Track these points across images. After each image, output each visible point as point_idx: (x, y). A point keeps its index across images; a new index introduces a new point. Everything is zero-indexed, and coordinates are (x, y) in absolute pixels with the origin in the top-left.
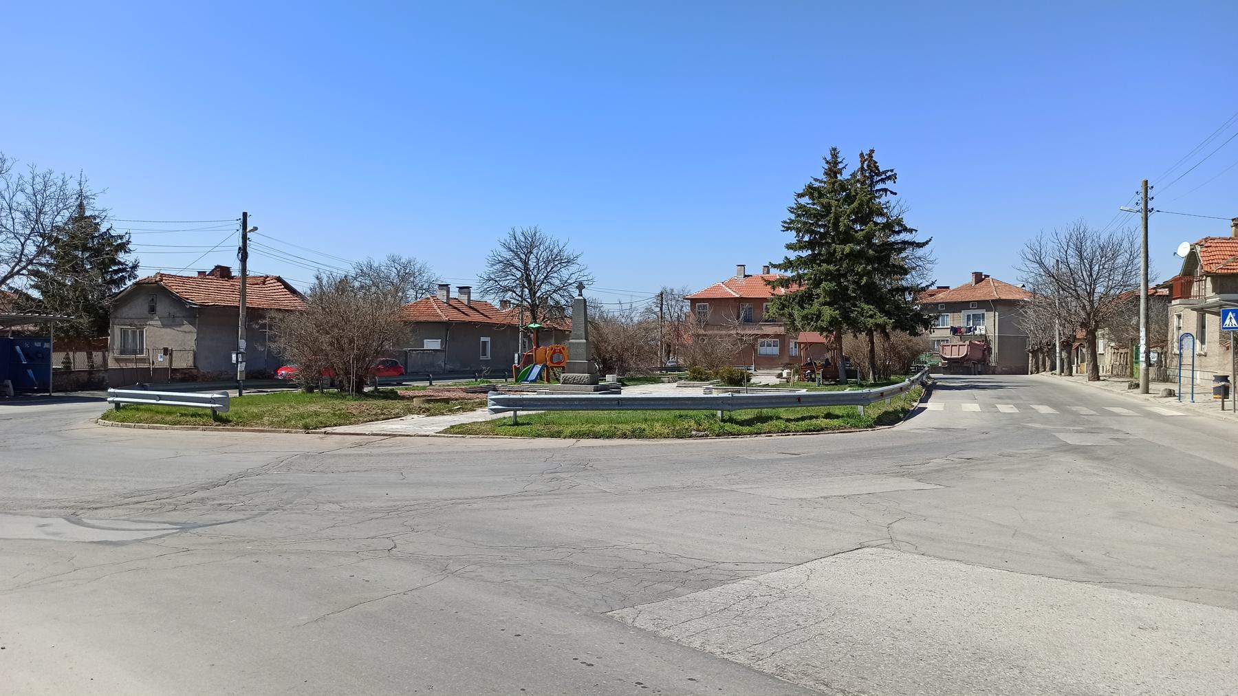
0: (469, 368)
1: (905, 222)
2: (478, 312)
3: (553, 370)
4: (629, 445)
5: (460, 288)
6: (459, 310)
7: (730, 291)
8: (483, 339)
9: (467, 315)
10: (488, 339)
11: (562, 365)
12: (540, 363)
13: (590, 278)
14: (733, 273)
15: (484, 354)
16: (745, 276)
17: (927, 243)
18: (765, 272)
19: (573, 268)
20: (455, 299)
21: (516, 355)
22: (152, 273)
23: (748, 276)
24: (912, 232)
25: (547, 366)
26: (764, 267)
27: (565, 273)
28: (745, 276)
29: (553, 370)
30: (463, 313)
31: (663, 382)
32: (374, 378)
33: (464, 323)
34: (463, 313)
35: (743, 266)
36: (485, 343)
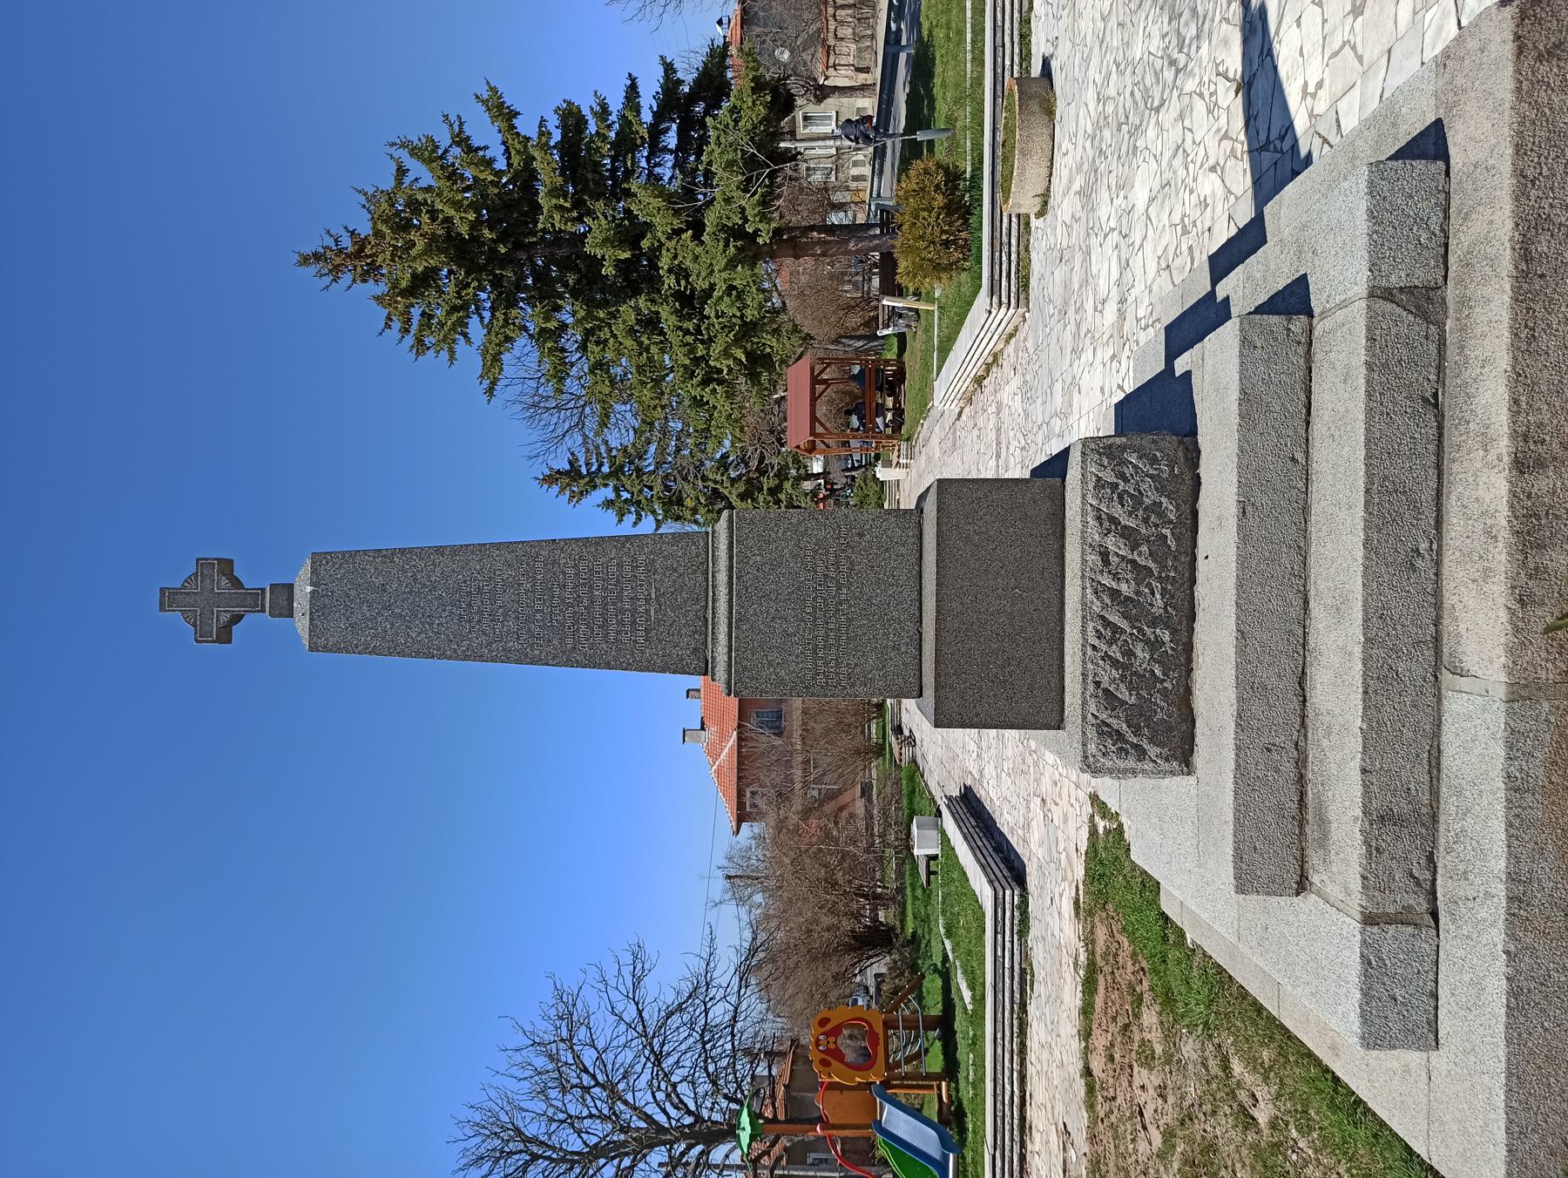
1: (484, 108)
3: (898, 1065)
4: (937, 661)
7: (726, 750)
11: (879, 1029)
12: (872, 1109)
13: (628, 959)
14: (697, 748)
16: (703, 728)
19: (591, 1001)
22: (698, 61)
23: (703, 724)
25: (886, 1084)
26: (688, 697)
27: (605, 1028)
28: (703, 728)
29: (898, 1065)
35: (684, 731)
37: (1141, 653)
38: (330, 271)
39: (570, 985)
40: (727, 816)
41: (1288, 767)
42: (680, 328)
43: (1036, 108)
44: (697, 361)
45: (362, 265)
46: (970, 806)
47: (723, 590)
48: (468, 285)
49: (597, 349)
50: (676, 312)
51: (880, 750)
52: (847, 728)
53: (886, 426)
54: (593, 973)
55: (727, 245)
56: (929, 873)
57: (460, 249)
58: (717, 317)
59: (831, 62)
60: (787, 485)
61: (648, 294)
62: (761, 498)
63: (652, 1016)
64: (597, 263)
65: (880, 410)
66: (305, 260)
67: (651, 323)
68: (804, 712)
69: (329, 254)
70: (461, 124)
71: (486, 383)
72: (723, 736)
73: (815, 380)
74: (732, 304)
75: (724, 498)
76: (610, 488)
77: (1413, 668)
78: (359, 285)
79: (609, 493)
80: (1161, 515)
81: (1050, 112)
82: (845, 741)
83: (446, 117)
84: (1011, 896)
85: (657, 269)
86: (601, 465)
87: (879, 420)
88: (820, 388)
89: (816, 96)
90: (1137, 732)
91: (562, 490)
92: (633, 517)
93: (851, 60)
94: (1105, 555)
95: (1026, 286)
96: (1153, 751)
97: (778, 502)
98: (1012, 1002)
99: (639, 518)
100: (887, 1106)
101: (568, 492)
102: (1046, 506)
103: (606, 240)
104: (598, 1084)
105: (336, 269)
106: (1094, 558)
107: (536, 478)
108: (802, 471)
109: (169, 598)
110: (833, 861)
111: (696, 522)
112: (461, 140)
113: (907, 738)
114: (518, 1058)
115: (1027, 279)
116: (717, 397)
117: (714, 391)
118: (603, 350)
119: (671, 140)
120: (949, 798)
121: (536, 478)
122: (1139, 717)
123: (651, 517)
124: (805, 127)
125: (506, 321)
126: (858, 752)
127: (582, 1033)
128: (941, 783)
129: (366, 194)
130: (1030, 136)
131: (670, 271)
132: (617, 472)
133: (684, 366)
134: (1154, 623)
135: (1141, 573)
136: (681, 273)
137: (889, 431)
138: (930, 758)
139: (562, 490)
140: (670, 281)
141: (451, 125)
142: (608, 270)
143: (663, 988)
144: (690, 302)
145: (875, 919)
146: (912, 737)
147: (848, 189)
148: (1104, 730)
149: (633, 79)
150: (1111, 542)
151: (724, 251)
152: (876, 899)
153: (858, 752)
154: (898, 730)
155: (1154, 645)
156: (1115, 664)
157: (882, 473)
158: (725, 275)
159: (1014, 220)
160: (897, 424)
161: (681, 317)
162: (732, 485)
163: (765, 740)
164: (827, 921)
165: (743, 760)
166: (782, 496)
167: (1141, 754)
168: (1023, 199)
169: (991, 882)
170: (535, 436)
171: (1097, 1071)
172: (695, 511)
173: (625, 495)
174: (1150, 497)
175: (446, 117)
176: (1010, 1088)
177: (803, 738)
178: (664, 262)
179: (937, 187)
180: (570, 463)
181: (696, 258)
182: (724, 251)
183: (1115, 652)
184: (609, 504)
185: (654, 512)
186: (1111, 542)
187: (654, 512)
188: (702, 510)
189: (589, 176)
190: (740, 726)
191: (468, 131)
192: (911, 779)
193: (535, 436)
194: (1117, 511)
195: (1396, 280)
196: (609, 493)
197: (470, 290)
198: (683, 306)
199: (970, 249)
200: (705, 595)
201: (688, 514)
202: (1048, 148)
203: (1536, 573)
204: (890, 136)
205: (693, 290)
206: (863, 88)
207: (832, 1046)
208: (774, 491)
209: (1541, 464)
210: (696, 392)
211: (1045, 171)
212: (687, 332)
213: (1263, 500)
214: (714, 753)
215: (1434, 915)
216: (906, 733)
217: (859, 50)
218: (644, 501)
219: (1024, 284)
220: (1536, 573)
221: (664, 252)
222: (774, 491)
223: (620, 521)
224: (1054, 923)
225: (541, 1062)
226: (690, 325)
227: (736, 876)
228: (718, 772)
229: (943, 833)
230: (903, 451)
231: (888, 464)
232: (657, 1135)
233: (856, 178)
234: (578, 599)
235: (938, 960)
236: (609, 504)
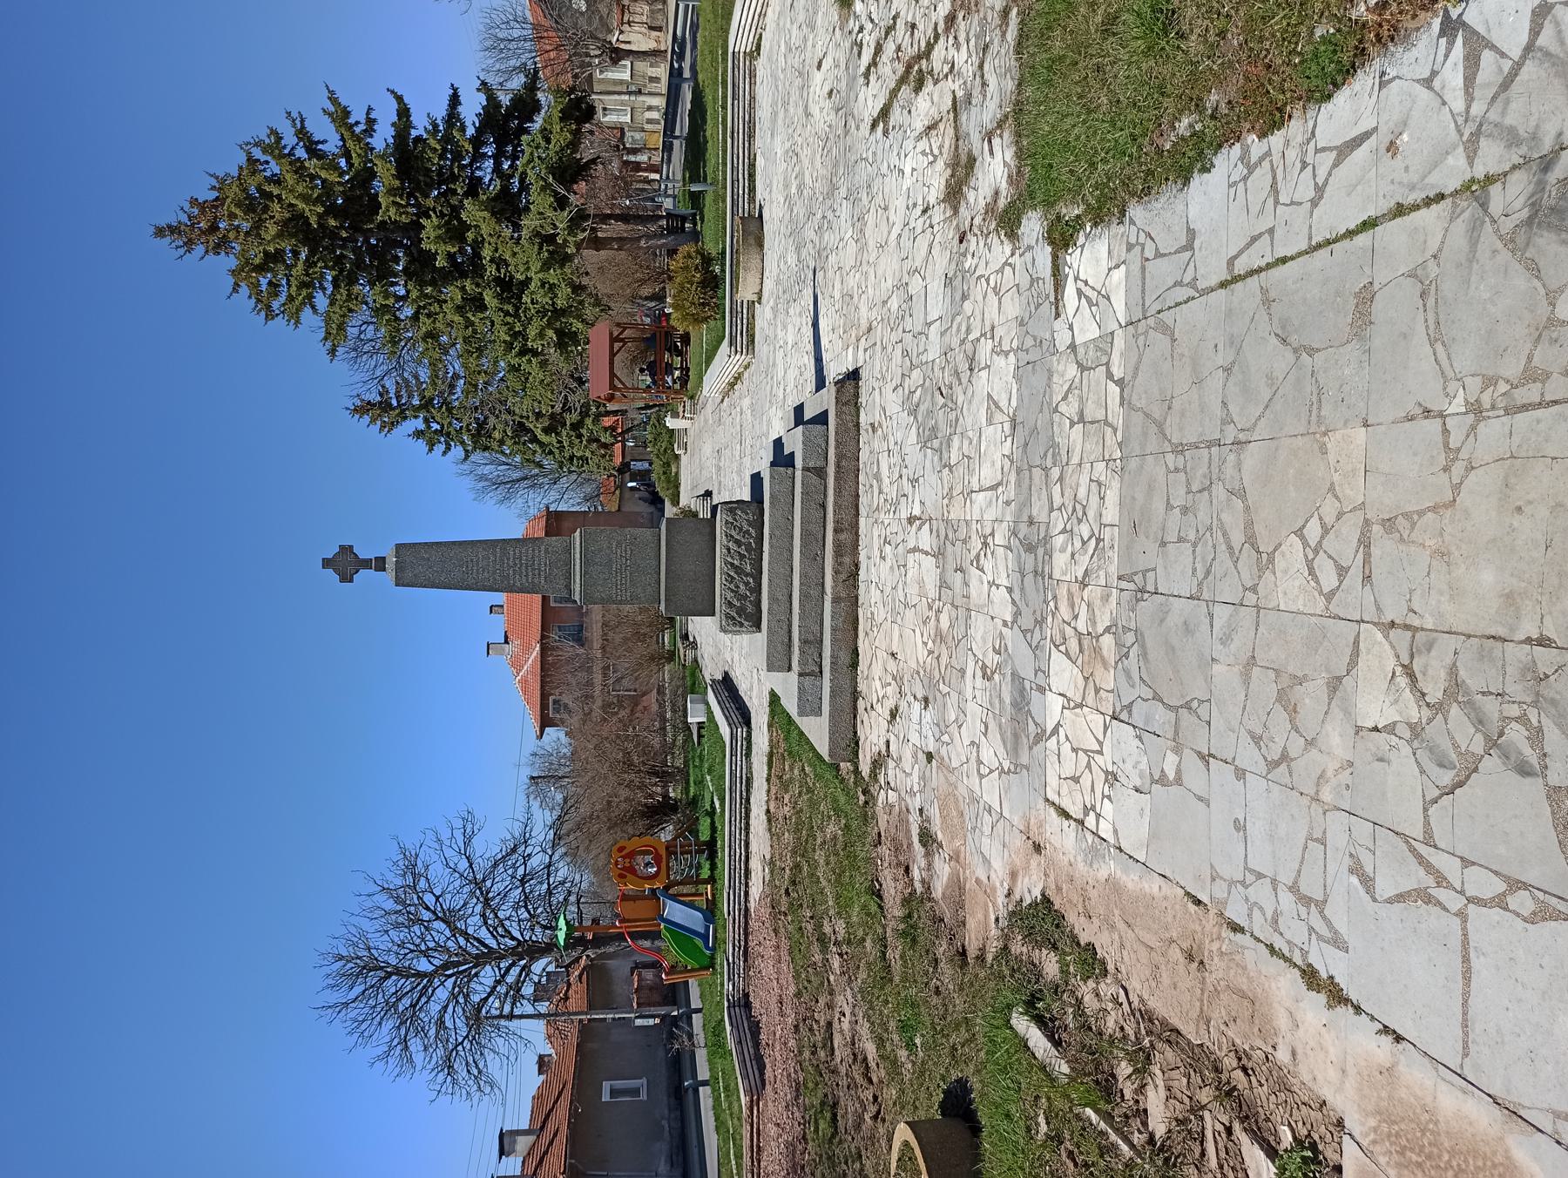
0: (665, 1123)
2: (551, 1110)
5: (502, 1152)
6: (546, 1153)
8: (606, 1097)
9: (555, 1135)
10: (606, 1086)
13: (459, 823)
15: (636, 1092)
17: (393, 92)
18: (500, 610)
19: (428, 855)
20: (523, 1162)
21: (639, 1022)
23: (506, 637)
24: (374, 121)
28: (506, 642)
30: (551, 1143)
31: (677, 474)
32: (669, 465)
33: (573, 1139)
34: (551, 1143)
36: (614, 1092)
37: (742, 587)
38: (185, 244)
39: (412, 848)
40: (533, 724)
41: (785, 627)
42: (501, 309)
43: (752, 241)
44: (515, 335)
45: (213, 239)
46: (727, 685)
47: (578, 561)
48: (315, 264)
49: (428, 321)
50: (498, 296)
51: (671, 656)
52: (640, 637)
53: (674, 382)
54: (430, 840)
55: (541, 248)
56: (700, 736)
57: (296, 225)
58: (533, 303)
59: (626, 19)
60: (589, 421)
61: (473, 278)
62: (564, 433)
63: (479, 877)
64: (432, 256)
65: (669, 369)
66: (160, 232)
67: (478, 304)
68: (605, 624)
69: (182, 228)
70: (302, 121)
71: (329, 344)
72: (527, 649)
73: (613, 340)
74: (545, 296)
75: (529, 431)
76: (421, 420)
77: (814, 593)
78: (211, 257)
79: (419, 424)
80: (750, 534)
81: (761, 245)
82: (641, 649)
83: (289, 114)
84: (741, 732)
85: (480, 258)
86: (410, 396)
87: (669, 380)
88: (617, 345)
89: (611, 58)
90: (740, 616)
91: (373, 421)
92: (442, 447)
93: (644, 19)
94: (729, 550)
95: (753, 341)
96: (746, 623)
97: (580, 436)
98: (741, 798)
99: (448, 448)
100: (669, 902)
101: (379, 423)
102: (708, 530)
103: (438, 237)
104: (438, 918)
105: (189, 244)
106: (724, 551)
107: (347, 409)
108: (602, 409)
109: (327, 563)
110: (630, 746)
111: (503, 453)
112: (302, 133)
113: (691, 643)
114: (369, 904)
115: (753, 336)
116: (532, 367)
117: (529, 361)
118: (434, 322)
119: (489, 150)
120: (713, 681)
121: (347, 409)
122: (741, 611)
123: (460, 448)
124: (605, 115)
125: (349, 295)
126: (652, 658)
127: (422, 884)
128: (711, 672)
129: (217, 178)
130: (749, 260)
131: (492, 261)
132: (427, 404)
133: (505, 342)
134: (747, 575)
135: (742, 557)
136: (499, 262)
137: (677, 386)
138: (706, 656)
139: (373, 421)
140: (491, 270)
141: (294, 121)
142: (440, 262)
143: (488, 846)
144: (510, 289)
145: (666, 796)
146: (695, 642)
147: (643, 130)
148: (728, 616)
149: (455, 90)
150: (730, 544)
151: (539, 253)
152: (664, 776)
153: (652, 658)
154: (685, 637)
155: (747, 584)
156: (732, 591)
157: (670, 423)
158: (540, 275)
159: (745, 305)
160: (684, 380)
161: (502, 300)
162: (537, 420)
163: (569, 649)
164: (624, 793)
165: (546, 668)
166: (584, 431)
167: (742, 625)
168: (746, 293)
169: (729, 725)
170: (358, 377)
171: (772, 810)
172: (502, 442)
173: (435, 426)
174: (746, 527)
175: (289, 114)
176: (739, 851)
177: (603, 648)
178: (487, 253)
179: (697, 268)
180: (381, 395)
181: (514, 254)
182: (539, 253)
183: (732, 586)
184: (418, 434)
185: (463, 443)
186: (730, 544)
187: (463, 443)
188: (509, 442)
189: (421, 178)
190: (543, 637)
191: (309, 126)
192: (693, 675)
193: (358, 377)
194: (733, 533)
195: (811, 464)
196: (419, 424)
197: (317, 269)
198: (503, 291)
199: (720, 308)
200: (569, 563)
201: (495, 445)
202: (760, 267)
203: (840, 564)
204: (677, 137)
205: (512, 277)
206: (655, 53)
207: (627, 865)
208: (576, 427)
209: (842, 531)
210: (515, 361)
211: (758, 281)
212: (507, 314)
213: (777, 533)
214: (517, 664)
215: (821, 672)
216: (691, 639)
217: (652, 11)
218: (453, 432)
219: (751, 340)
220: (840, 564)
221: (486, 245)
222: (576, 427)
223: (431, 450)
224: (760, 741)
225: (390, 905)
226: (510, 308)
227: (539, 777)
228: (524, 682)
229: (707, 704)
230: (688, 408)
231: (675, 415)
232: (488, 956)
233: (650, 121)
234: (515, 564)
235: (708, 807)
236: (418, 434)
